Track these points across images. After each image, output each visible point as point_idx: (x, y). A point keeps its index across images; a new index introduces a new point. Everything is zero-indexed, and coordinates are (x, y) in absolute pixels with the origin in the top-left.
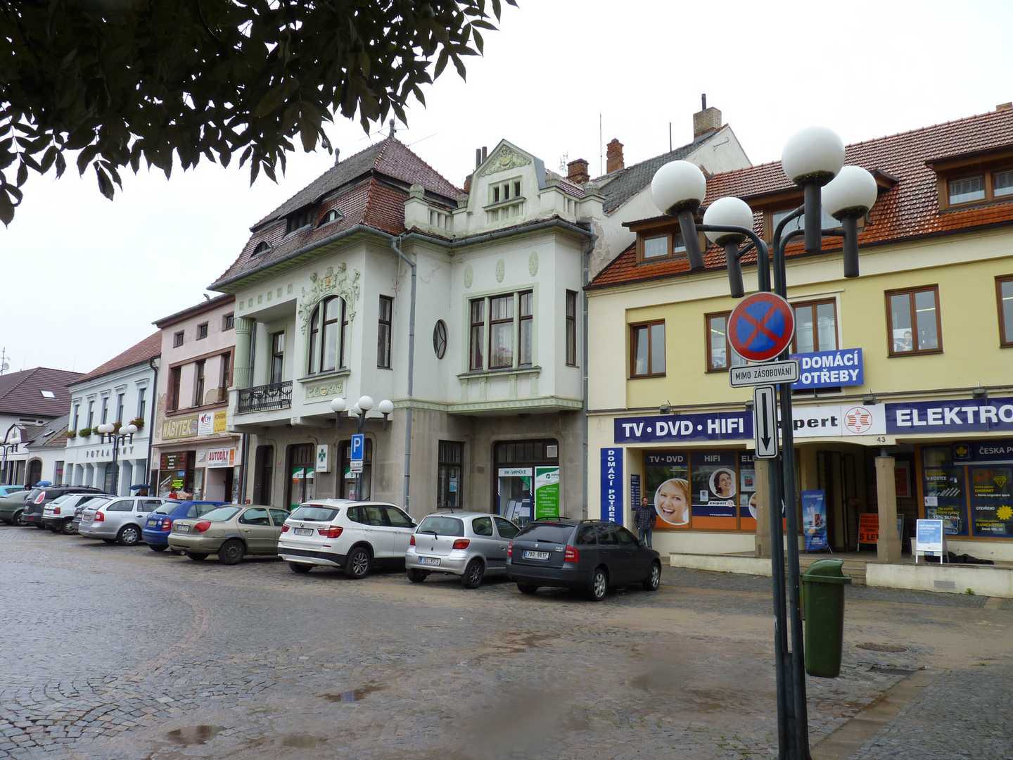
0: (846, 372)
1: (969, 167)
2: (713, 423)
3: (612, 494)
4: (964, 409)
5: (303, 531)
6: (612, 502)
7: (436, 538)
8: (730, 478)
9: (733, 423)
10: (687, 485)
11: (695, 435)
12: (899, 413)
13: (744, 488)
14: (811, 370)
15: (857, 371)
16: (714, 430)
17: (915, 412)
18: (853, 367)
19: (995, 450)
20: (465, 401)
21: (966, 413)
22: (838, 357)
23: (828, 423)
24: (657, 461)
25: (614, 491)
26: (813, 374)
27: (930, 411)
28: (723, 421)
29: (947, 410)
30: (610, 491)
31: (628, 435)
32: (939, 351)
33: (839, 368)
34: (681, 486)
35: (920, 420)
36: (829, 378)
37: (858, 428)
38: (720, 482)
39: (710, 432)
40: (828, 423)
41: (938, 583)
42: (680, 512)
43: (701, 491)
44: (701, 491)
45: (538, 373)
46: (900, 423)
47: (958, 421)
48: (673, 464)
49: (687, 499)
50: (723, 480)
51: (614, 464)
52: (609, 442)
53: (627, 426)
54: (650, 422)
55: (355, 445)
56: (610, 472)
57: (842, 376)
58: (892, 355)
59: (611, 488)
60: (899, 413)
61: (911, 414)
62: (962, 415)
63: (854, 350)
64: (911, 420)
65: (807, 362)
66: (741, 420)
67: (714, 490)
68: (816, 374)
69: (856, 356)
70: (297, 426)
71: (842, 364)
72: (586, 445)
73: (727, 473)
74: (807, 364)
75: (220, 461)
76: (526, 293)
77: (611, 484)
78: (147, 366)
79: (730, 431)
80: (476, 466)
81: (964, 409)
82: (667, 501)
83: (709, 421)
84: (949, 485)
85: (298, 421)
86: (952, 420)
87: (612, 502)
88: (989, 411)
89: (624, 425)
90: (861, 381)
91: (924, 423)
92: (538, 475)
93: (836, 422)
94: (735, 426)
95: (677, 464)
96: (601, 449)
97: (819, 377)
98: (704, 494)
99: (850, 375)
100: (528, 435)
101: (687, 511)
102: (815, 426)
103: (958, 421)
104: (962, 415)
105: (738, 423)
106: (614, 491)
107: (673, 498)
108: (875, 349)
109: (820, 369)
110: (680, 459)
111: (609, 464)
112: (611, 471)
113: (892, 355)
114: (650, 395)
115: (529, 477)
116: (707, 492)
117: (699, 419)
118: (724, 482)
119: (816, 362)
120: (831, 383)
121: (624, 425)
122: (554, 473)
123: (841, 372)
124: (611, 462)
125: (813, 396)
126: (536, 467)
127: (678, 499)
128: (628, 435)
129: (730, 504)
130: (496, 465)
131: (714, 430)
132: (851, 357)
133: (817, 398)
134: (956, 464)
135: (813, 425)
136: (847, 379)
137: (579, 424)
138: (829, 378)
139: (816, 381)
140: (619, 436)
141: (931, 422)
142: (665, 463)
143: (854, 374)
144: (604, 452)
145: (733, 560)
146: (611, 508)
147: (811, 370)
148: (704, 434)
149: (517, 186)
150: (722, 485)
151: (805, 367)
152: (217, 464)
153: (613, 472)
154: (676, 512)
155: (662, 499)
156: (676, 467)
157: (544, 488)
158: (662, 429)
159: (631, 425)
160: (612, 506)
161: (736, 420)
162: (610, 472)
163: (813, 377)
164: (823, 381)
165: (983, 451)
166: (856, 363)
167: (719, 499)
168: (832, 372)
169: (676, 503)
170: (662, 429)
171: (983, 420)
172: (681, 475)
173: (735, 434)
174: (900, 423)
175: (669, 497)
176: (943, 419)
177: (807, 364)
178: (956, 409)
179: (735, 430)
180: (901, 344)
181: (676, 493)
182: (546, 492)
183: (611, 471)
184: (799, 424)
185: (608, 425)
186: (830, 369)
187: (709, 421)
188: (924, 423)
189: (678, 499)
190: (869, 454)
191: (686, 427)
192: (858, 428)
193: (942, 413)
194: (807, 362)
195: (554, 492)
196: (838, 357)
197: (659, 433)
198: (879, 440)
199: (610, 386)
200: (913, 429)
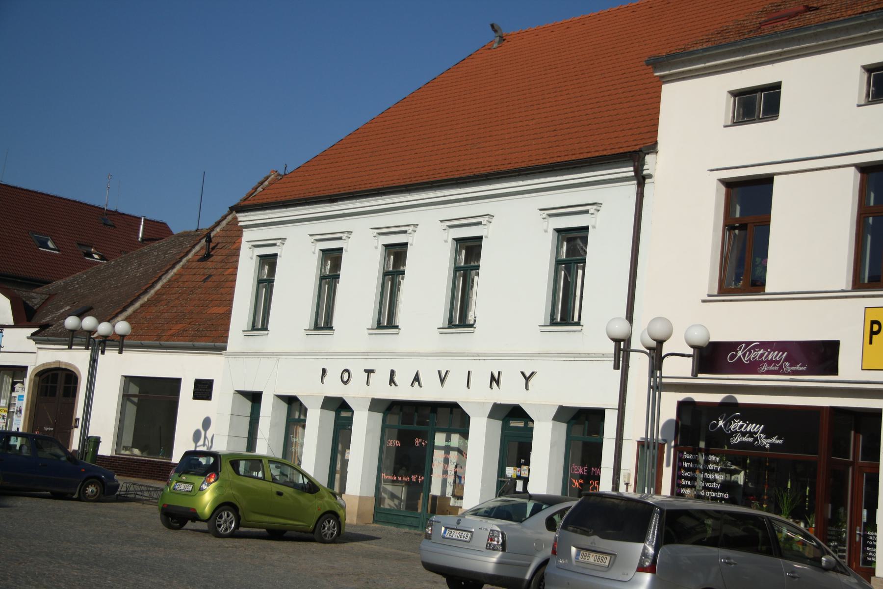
78: (628, 171)
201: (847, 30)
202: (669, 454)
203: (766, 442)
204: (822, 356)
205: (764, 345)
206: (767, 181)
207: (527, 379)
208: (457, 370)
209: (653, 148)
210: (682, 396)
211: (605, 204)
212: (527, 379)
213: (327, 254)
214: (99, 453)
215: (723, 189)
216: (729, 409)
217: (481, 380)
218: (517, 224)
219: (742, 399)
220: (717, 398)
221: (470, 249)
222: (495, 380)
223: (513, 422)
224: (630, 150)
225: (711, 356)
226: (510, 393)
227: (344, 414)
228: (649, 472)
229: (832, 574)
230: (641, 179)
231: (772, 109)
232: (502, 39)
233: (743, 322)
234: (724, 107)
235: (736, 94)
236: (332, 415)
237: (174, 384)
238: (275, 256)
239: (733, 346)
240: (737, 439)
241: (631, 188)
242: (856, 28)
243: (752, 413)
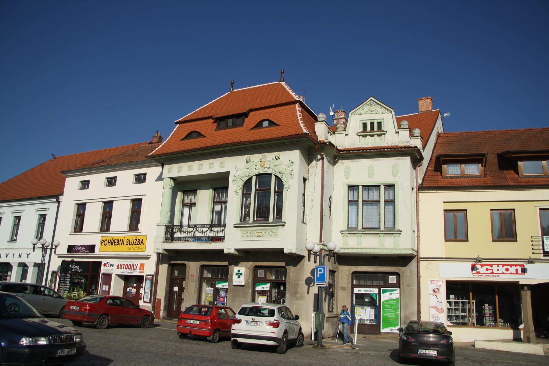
5: (253, 323)
20: (346, 247)
45: (400, 234)
55: (319, 273)
70: (229, 255)
75: (129, 271)
76: (391, 187)
78: (55, 200)
80: (340, 286)
85: (232, 251)
92: (383, 293)
108: (405, 194)
115: (376, 294)
126: (382, 289)
130: (353, 286)
145: (496, 343)
149: (379, 124)
152: (126, 272)
157: (387, 301)
199: (432, 240)
200: (511, 265)
201: (102, 169)
202: (59, 274)
203: (79, 271)
204: (91, 248)
205: (81, 246)
206: (112, 202)
207: (28, 255)
208: (11, 253)
209: (62, 194)
210: (63, 259)
211: (50, 207)
212: (28, 255)
213: (41, 216)
214: (122, 296)
215: (77, 206)
216: (72, 262)
217: (17, 256)
218: (30, 212)
219: (75, 260)
220: (70, 259)
221: (18, 218)
222: (20, 256)
223: (24, 266)
224: (56, 194)
225: (71, 249)
226: (23, 260)
227: (26, 268)
228: (53, 280)
229: (57, 299)
230: (59, 202)
231: (144, 181)
232: (55, 158)
233: (80, 240)
234: (132, 179)
235: (136, 175)
236: (21, 269)
237: (101, 263)
238: (20, 216)
239: (74, 246)
240: (73, 270)
241: (56, 204)
242: (104, 169)
243: (77, 263)
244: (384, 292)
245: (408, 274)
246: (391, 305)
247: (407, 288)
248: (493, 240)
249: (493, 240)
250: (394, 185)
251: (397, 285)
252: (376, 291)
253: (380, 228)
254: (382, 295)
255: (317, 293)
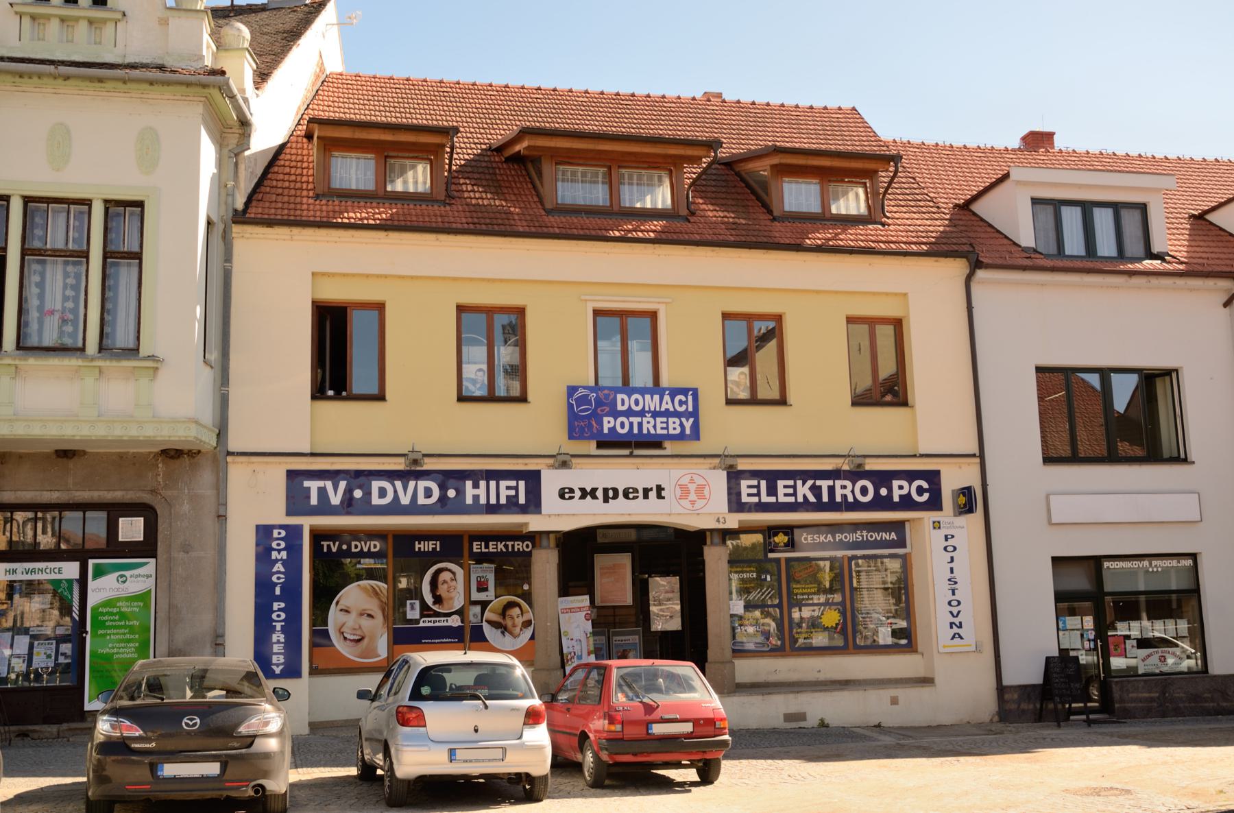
0: (677, 420)
1: (414, 144)
2: (476, 486)
3: (279, 610)
4: (818, 483)
6: (278, 626)
7: (486, 707)
8: (454, 579)
9: (508, 488)
10: (385, 592)
11: (444, 505)
12: (744, 483)
13: (476, 596)
14: (629, 413)
15: (691, 420)
16: (476, 498)
17: (763, 483)
18: (687, 415)
19: (822, 538)
21: (820, 487)
22: (667, 398)
23: (653, 494)
24: (334, 550)
25: (283, 605)
26: (631, 419)
27: (781, 483)
28: (493, 484)
29: (799, 483)
30: (276, 606)
31: (314, 501)
32: (380, 397)
33: (667, 414)
34: (375, 593)
35: (768, 495)
36: (655, 427)
37: (693, 503)
38: (440, 586)
39: (469, 501)
40: (653, 494)
41: (789, 717)
42: (373, 639)
43: (408, 602)
44: (408, 602)
46: (745, 499)
47: (812, 499)
48: (362, 554)
49: (385, 617)
50: (445, 582)
51: (284, 555)
52: (276, 514)
53: (313, 485)
54: (361, 477)
56: (275, 569)
57: (671, 426)
58: (461, 399)
59: (278, 599)
60: (744, 483)
61: (758, 487)
62: (816, 490)
63: (689, 390)
64: (758, 494)
65: (623, 401)
66: (522, 484)
67: (429, 599)
68: (635, 420)
69: (690, 398)
71: (672, 409)
72: (222, 518)
73: (450, 570)
74: (623, 404)
77: (278, 591)
79: (503, 501)
81: (818, 483)
82: (350, 620)
83: (469, 484)
84: (760, 582)
86: (804, 496)
87: (278, 626)
88: (844, 487)
89: (306, 484)
90: (696, 434)
91: (773, 499)
93: (663, 493)
94: (512, 493)
95: (369, 555)
96: (258, 527)
97: (640, 424)
98: (412, 608)
99: (681, 425)
100: (78, 493)
101: (386, 636)
102: (571, 498)
103: (812, 499)
104: (816, 490)
105: (516, 488)
106: (283, 605)
107: (362, 615)
109: (642, 414)
110: (375, 546)
111: (274, 555)
112: (279, 567)
113: (461, 399)
114: (350, 428)
115: (70, 582)
116: (417, 603)
117: (448, 478)
118: (445, 586)
119: (637, 403)
120: (656, 435)
121: (306, 484)
122: (136, 572)
123: (671, 420)
124: (279, 551)
125: (627, 452)
126: (91, 562)
127: (370, 616)
128: (314, 501)
129: (455, 621)
131: (476, 498)
132: (684, 399)
133: (631, 455)
134: (771, 555)
135: (631, 496)
136: (678, 431)
137: (206, 477)
138: (655, 427)
139: (636, 431)
140: (296, 502)
141: (782, 499)
142: (348, 554)
143: (688, 424)
144: (264, 532)
146: (278, 637)
147: (629, 413)
148: (459, 507)
150: (442, 590)
151: (620, 407)
153: (282, 569)
154: (366, 641)
155: (342, 617)
156: (367, 560)
157: (108, 603)
158: (382, 493)
159: (321, 484)
160: (278, 634)
161: (513, 483)
162: (275, 569)
163: (631, 424)
164: (645, 431)
165: (806, 539)
166: (690, 409)
167: (437, 614)
168: (659, 420)
169: (365, 623)
170: (382, 493)
171: (838, 499)
172: (371, 574)
173: (512, 505)
174: (745, 499)
175: (354, 615)
176: (795, 494)
177: (623, 404)
178: (810, 483)
179: (513, 500)
180: (736, 389)
181: (367, 606)
182: (115, 610)
183: (279, 567)
184: (611, 493)
185: (274, 476)
186: (655, 414)
187: (469, 484)
188: (773, 499)
189: (370, 616)
190: (698, 538)
191: (424, 491)
192: (693, 503)
193: (794, 487)
194: (623, 401)
195: (136, 617)
196: (667, 398)
197: (376, 500)
198: (718, 520)
199: (277, 404)
244: (100, 572)
245: (186, 507)
246: (123, 616)
247: (181, 555)
248: (1048, 460)
249: (1048, 460)
250: (140, 204)
251: (147, 548)
252: (71, 570)
253: (83, 349)
254: (91, 584)
255: (1140, 672)
